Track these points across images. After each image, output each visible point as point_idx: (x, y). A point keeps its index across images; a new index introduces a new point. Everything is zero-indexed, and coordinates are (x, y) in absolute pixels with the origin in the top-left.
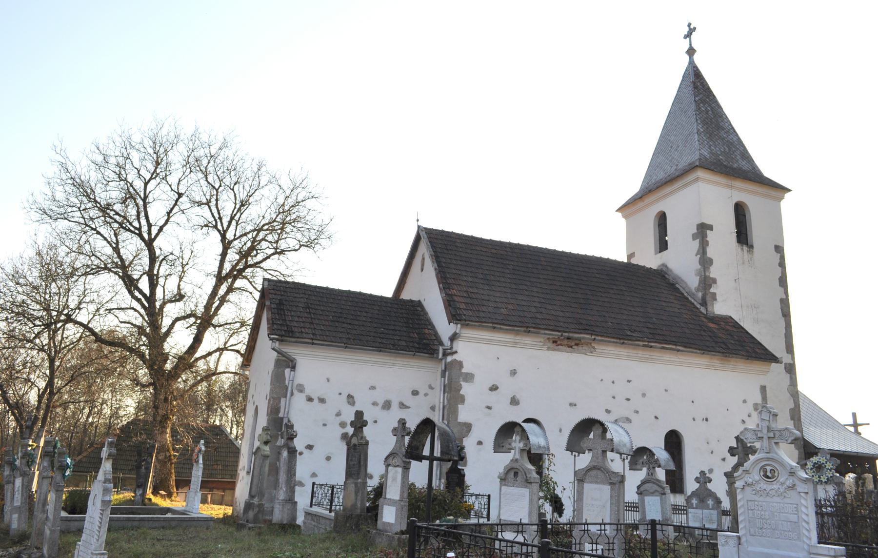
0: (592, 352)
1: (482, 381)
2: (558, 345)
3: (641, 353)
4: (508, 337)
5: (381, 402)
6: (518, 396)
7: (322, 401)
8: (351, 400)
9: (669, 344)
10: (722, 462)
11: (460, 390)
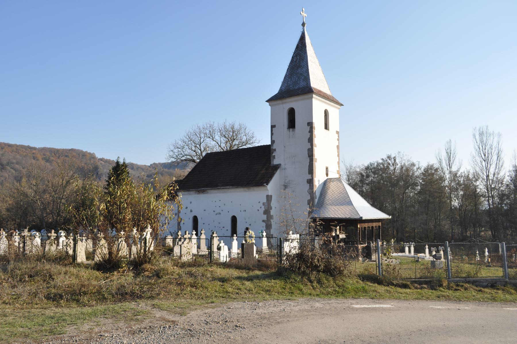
3: (223, 190)
6: (192, 210)
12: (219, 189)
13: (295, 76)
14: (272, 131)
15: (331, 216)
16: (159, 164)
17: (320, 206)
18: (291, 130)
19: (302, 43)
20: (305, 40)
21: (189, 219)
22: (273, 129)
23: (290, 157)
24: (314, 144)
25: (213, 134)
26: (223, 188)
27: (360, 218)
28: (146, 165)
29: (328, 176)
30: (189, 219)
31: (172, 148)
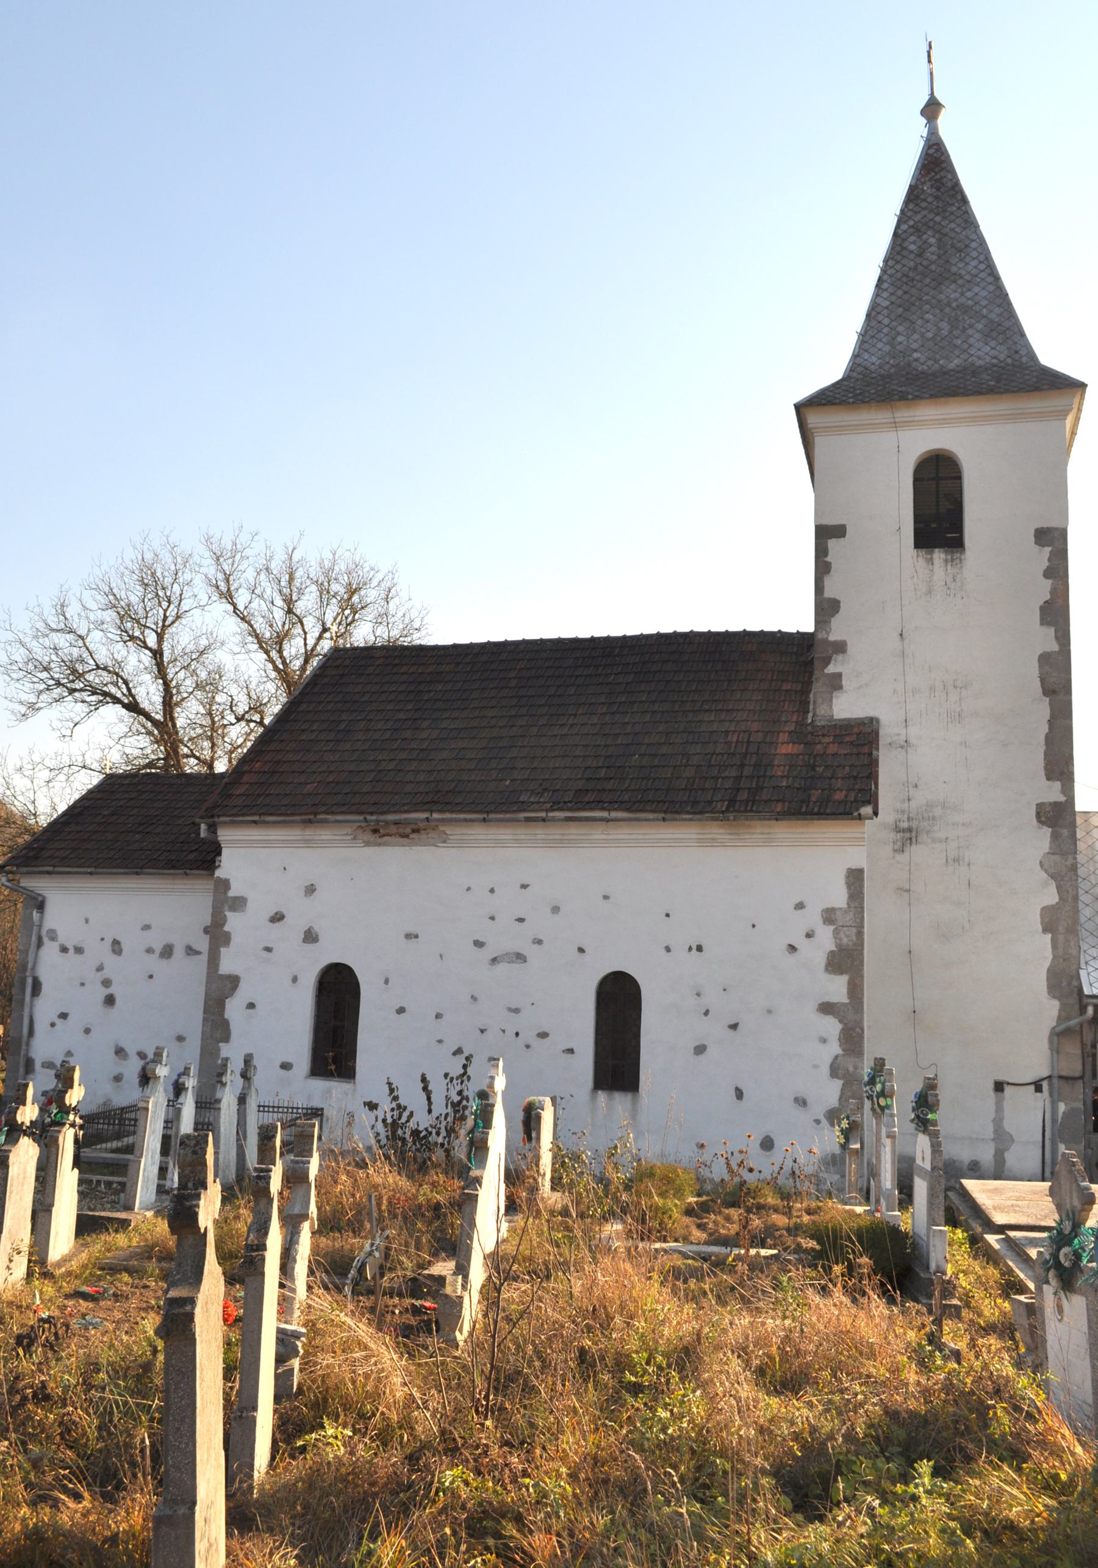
0: (445, 842)
1: (258, 909)
2: (384, 836)
4: (293, 833)
5: (158, 947)
6: (316, 928)
7: (79, 950)
8: (116, 947)
9: (592, 809)
11: (223, 925)
14: (821, 552)
18: (939, 555)
22: (832, 544)
30: (295, 980)
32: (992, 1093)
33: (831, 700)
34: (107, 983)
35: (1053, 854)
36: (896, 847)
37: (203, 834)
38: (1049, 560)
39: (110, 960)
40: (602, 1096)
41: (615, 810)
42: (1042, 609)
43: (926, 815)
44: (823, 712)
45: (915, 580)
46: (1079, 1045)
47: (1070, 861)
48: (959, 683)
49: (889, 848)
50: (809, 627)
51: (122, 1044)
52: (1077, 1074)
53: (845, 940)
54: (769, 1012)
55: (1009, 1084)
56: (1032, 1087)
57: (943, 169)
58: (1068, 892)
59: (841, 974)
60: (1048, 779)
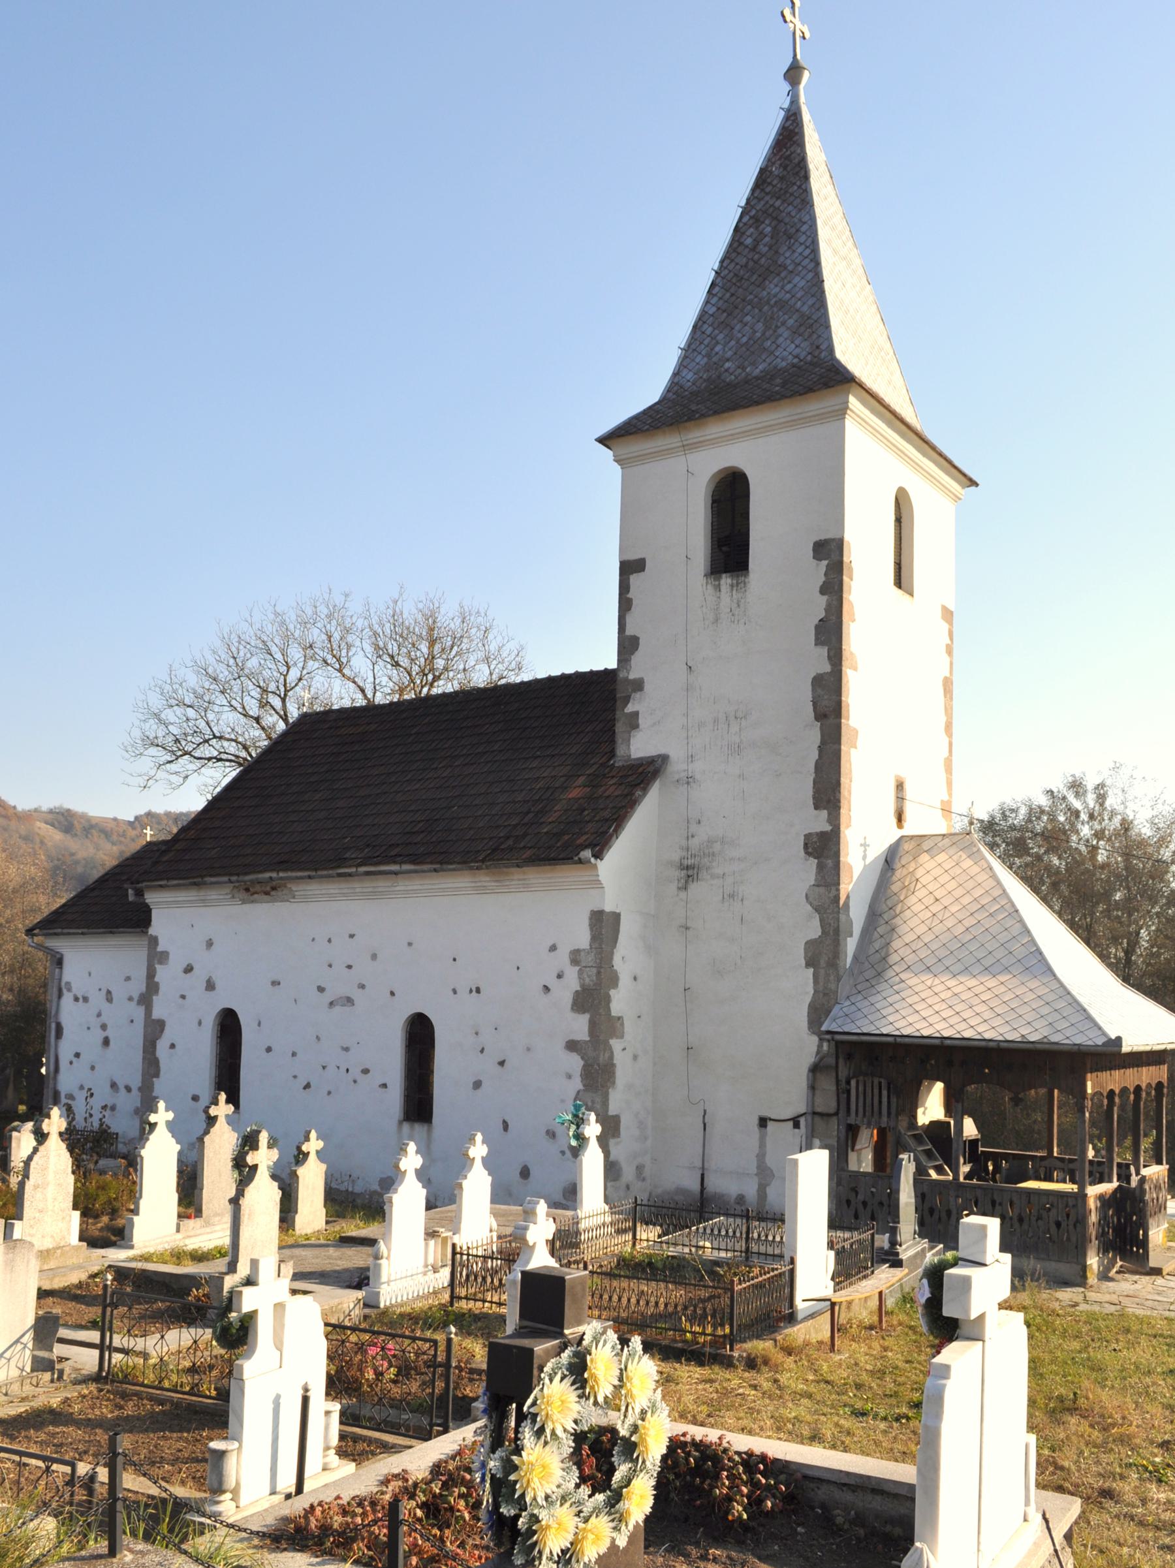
3: (369, 885)
7: (86, 999)
10: (500, 1067)
12: (350, 875)
13: (748, 318)
14: (624, 588)
15: (897, 1025)
16: (168, 814)
17: (868, 975)
18: (726, 580)
19: (788, 158)
20: (802, 145)
21: (200, 1023)
22: (634, 579)
23: (716, 721)
24: (845, 654)
25: (344, 653)
26: (368, 873)
27: (1104, 1044)
28: (120, 817)
29: (905, 824)
30: (200, 1023)
31: (156, 702)
32: (756, 1128)
33: (629, 740)
34: (104, 1027)
35: (818, 886)
36: (680, 885)
37: (131, 898)
38: (826, 574)
39: (105, 1006)
40: (406, 1127)
41: (405, 862)
42: (818, 628)
43: (706, 851)
44: (622, 752)
45: (704, 608)
46: (834, 1080)
47: (833, 892)
48: (740, 714)
49: (673, 887)
50: (612, 664)
51: (115, 1080)
52: (832, 1111)
53: (587, 980)
54: (528, 1049)
55: (771, 1119)
56: (791, 1124)
57: (794, 142)
58: (830, 924)
59: (584, 1013)
60: (816, 807)
